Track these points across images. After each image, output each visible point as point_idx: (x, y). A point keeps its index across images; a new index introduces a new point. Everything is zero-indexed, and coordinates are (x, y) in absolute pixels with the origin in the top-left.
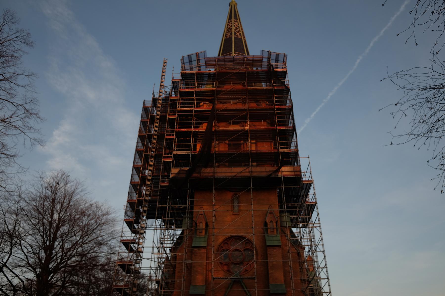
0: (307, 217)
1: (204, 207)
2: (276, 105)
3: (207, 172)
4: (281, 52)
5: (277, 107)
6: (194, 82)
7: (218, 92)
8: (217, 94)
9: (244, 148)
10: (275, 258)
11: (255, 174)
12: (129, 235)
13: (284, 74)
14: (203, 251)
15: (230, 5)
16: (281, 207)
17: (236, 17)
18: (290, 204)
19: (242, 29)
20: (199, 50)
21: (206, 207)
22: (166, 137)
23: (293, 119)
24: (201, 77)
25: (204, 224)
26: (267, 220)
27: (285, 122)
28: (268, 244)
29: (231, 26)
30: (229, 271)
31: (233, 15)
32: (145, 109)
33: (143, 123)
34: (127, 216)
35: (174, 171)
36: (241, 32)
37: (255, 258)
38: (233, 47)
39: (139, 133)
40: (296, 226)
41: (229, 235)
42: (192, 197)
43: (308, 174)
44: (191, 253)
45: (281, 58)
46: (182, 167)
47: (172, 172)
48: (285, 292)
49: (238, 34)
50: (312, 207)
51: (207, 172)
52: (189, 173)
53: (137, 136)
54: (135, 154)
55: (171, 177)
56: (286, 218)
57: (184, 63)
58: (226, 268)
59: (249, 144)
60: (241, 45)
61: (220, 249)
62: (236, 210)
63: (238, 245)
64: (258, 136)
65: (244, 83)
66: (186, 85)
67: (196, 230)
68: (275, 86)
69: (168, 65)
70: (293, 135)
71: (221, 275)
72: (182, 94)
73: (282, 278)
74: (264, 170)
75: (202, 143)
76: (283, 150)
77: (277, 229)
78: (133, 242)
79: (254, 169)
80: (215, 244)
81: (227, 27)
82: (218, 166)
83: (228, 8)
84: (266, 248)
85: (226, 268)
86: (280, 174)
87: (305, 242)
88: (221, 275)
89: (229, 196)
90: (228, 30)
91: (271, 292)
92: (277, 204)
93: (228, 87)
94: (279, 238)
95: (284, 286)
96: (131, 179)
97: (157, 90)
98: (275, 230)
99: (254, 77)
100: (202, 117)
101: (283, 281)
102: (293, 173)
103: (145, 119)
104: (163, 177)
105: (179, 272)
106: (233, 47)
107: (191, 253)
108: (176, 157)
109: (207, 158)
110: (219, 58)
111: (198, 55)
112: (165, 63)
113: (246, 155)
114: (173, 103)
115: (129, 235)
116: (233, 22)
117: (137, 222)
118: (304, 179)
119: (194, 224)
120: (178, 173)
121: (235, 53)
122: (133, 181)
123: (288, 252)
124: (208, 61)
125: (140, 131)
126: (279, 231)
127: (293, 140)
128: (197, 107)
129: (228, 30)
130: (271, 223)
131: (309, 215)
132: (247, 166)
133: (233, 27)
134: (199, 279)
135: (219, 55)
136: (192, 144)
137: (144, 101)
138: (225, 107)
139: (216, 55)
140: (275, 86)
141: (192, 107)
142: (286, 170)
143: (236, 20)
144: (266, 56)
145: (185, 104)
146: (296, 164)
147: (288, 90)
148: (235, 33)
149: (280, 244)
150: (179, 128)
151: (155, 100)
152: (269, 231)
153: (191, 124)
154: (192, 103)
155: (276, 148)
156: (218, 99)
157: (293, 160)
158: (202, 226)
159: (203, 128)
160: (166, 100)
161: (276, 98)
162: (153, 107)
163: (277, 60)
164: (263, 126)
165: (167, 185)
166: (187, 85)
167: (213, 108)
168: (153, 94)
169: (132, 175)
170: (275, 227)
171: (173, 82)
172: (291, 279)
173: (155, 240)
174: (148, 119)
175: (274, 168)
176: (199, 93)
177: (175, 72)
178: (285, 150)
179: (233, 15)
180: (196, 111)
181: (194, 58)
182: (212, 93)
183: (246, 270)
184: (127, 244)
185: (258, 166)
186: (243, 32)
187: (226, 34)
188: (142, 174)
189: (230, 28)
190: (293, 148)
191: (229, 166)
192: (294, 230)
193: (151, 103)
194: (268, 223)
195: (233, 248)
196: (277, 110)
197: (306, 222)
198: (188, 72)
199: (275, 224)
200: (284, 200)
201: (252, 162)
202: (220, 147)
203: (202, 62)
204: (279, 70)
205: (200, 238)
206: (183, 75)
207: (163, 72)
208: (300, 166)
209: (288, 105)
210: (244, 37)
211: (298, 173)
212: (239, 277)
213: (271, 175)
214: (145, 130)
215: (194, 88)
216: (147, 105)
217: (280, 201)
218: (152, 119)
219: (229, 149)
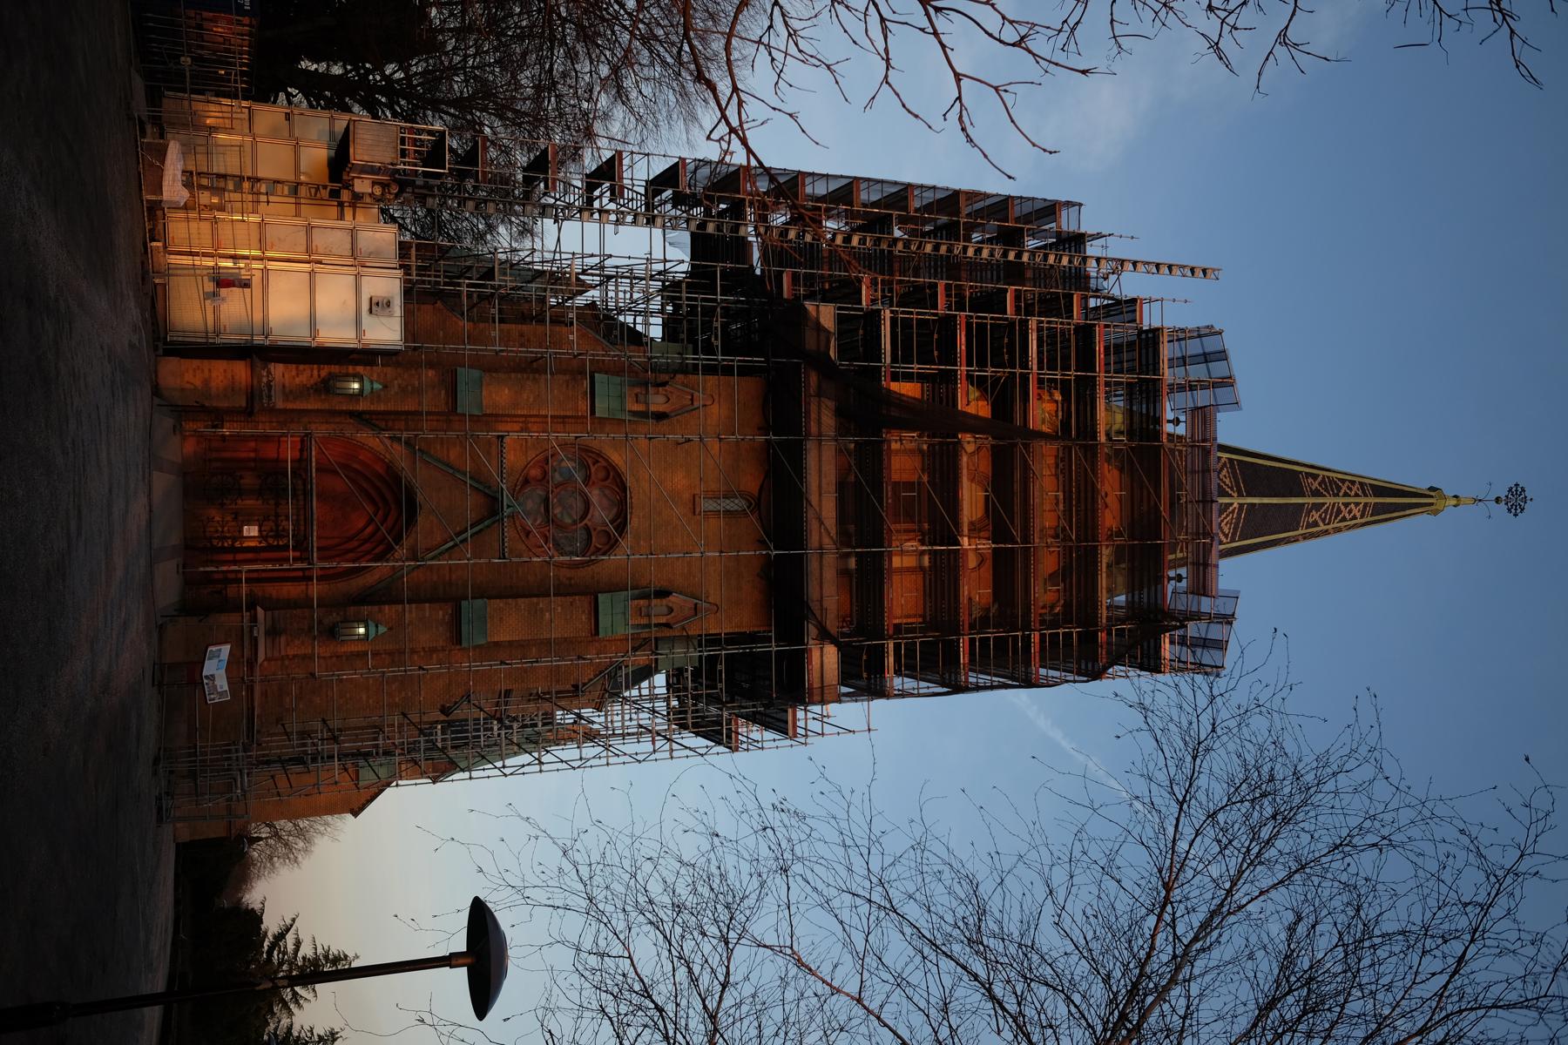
0: (690, 721)
1: (716, 405)
2: (1042, 636)
3: (823, 417)
4: (1231, 657)
5: (1035, 637)
6: (1130, 371)
7: (1091, 451)
8: (1085, 448)
9: (898, 531)
10: (561, 620)
11: (813, 565)
12: (638, 173)
13: (1152, 664)
14: (584, 406)
15: (1432, 489)
16: (714, 640)
17: (1379, 509)
18: (722, 667)
19: (1338, 530)
20: (1244, 387)
21: (717, 412)
22: (941, 284)
23: (992, 688)
24: (1146, 397)
25: (661, 409)
26: (675, 599)
27: (981, 662)
28: (601, 597)
29: (1346, 495)
30: (526, 481)
31: (1390, 501)
32: (1050, 210)
33: (1002, 206)
34: (696, 168)
35: (827, 315)
36: (1322, 527)
38: (1266, 500)
39: (967, 193)
42: (745, 371)
43: (815, 726)
44: (575, 372)
45: (1207, 657)
46: (838, 339)
48: (464, 644)
49: (1315, 515)
50: (719, 734)
51: (823, 417)
53: (956, 185)
54: (896, 183)
55: (809, 306)
56: (685, 656)
57: (1200, 336)
58: (535, 472)
59: (911, 545)
60: (1265, 528)
61: (589, 458)
62: (707, 505)
63: (601, 513)
64: (942, 576)
65: (1119, 534)
66: (1116, 346)
67: (645, 384)
68: (1109, 634)
69: (1199, 281)
70: (943, 686)
71: (513, 458)
72: (1086, 333)
73: (503, 637)
74: (827, 590)
75: (920, 401)
76: (891, 653)
77: (648, 626)
78: (616, 193)
79: (830, 559)
80: (602, 441)
81: (1343, 481)
82: (839, 451)
83: (1422, 485)
84: (592, 593)
85: (535, 472)
88: (513, 458)
89: (750, 481)
90: (1333, 483)
91: (464, 604)
92: (725, 629)
93: (1110, 483)
94: (621, 631)
95: (482, 642)
96: (812, 174)
97: (1116, 249)
98: (644, 621)
99: (1144, 564)
100: (1006, 398)
102: (816, 684)
103: (1016, 211)
105: (522, 335)
106: (1266, 500)
107: (575, 372)
108: (873, 318)
109: (868, 415)
110: (1215, 448)
111: (1227, 382)
112: (1204, 271)
113: (877, 536)
114: (1054, 306)
115: (638, 173)
116: (1363, 500)
117: (677, 200)
118: (800, 714)
119: (665, 377)
120: (819, 327)
121: (1241, 505)
122: (808, 180)
123: (579, 658)
124: (1202, 417)
125: (973, 196)
126: (644, 633)
127: (923, 684)
129: (1332, 481)
130: (665, 610)
132: (844, 538)
133: (1341, 500)
134: (499, 395)
135: (1223, 448)
136: (915, 368)
138: (1046, 472)
139: (1222, 439)
140: (1109, 634)
142: (825, 660)
143: (1369, 510)
144: (1222, 607)
145: (1053, 344)
146: (844, 690)
148: (1317, 507)
150: (969, 326)
151: (1077, 241)
152: (642, 602)
153: (982, 364)
154: (1052, 367)
155: (897, 628)
157: (863, 683)
158: (657, 402)
159: (972, 403)
160: (1079, 279)
161: (1068, 636)
162: (1059, 234)
163: (1205, 643)
164: (975, 590)
165: (785, 296)
167: (1040, 435)
168: (1099, 236)
169: (827, 176)
170: (654, 621)
171: (1134, 301)
172: (502, 663)
174: (1017, 220)
175: (832, 625)
176: (1087, 385)
177: (1169, 307)
178: (891, 659)
179: (1390, 501)
180: (1025, 379)
181: (1218, 369)
182: (1088, 429)
183: (528, 533)
184: (609, 171)
185: (844, 573)
186: (1326, 533)
187: (1315, 477)
188: (827, 210)
189: (1339, 488)
190: (897, 682)
191: (841, 486)
192: (660, 680)
193: (1073, 228)
194: (664, 601)
195: (595, 495)
196: (1027, 641)
197: (680, 719)
198: (1167, 351)
199: (663, 620)
202: (904, 455)
203: (1202, 398)
204: (1167, 650)
205: (622, 397)
206: (1156, 332)
207: (1170, 267)
208: (840, 702)
209: (1043, 671)
210: (1306, 537)
211: (817, 698)
212: (507, 511)
214: (979, 213)
215: (1108, 372)
216: (1064, 213)
217: (733, 639)
218: (1011, 238)
219: (896, 484)
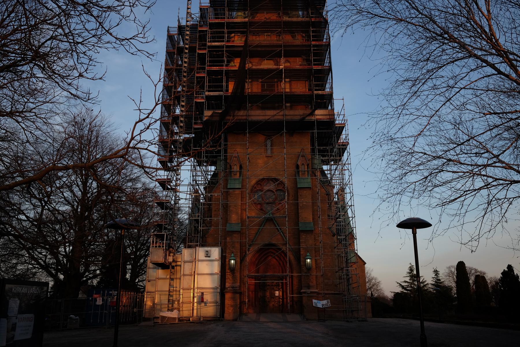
2: (313, 41)
5: (313, 43)
9: (278, 89)
10: (305, 199)
11: (289, 118)
12: (163, 174)
14: (237, 191)
16: (313, 151)
23: (330, 58)
27: (321, 61)
30: (262, 209)
32: (170, 37)
35: (208, 113)
37: (286, 198)
40: (327, 163)
41: (261, 177)
42: (226, 140)
43: (341, 117)
47: (205, 115)
48: (313, 229)
51: (241, 114)
52: (223, 116)
56: (318, 159)
58: (259, 207)
61: (254, 190)
63: (272, 186)
64: (293, 75)
65: (279, 14)
67: (231, 172)
68: (312, 17)
74: (297, 113)
76: (318, 92)
77: (308, 171)
79: (287, 112)
80: (249, 186)
85: (259, 207)
86: (313, 118)
87: (336, 182)
89: (261, 138)
91: (300, 229)
98: (306, 173)
100: (234, 53)
101: (312, 219)
104: (196, 119)
105: (215, 211)
107: (227, 194)
108: (208, 98)
109: (239, 100)
114: (202, 37)
118: (337, 122)
120: (211, 116)
123: (318, 193)
125: (166, 64)
126: (310, 173)
128: (228, 41)
130: (303, 166)
131: (340, 156)
132: (280, 108)
134: (234, 218)
136: (224, 84)
137: (168, 27)
140: (312, 17)
141: (223, 41)
142: (320, 114)
147: (326, 22)
149: (311, 186)
151: (181, 28)
152: (300, 173)
154: (223, 37)
155: (309, 90)
156: (250, 31)
158: (236, 168)
159: (235, 65)
160: (193, 28)
161: (313, 32)
164: (297, 63)
166: (216, 14)
167: (246, 41)
168: (179, 21)
170: (306, 170)
172: (319, 217)
173: (188, 175)
174: (174, 49)
175: (308, 112)
178: (320, 92)
180: (227, 47)
182: (244, 25)
183: (278, 209)
185: (291, 108)
190: (328, 90)
193: (176, 29)
195: (266, 188)
196: (314, 46)
197: (338, 160)
199: (306, 167)
200: (316, 144)
201: (285, 79)
202: (253, 88)
208: (334, 109)
209: (325, 40)
212: (271, 216)
213: (304, 118)
214: (172, 62)
216: (171, 33)
217: (313, 144)
218: (180, 51)
219: (262, 90)
